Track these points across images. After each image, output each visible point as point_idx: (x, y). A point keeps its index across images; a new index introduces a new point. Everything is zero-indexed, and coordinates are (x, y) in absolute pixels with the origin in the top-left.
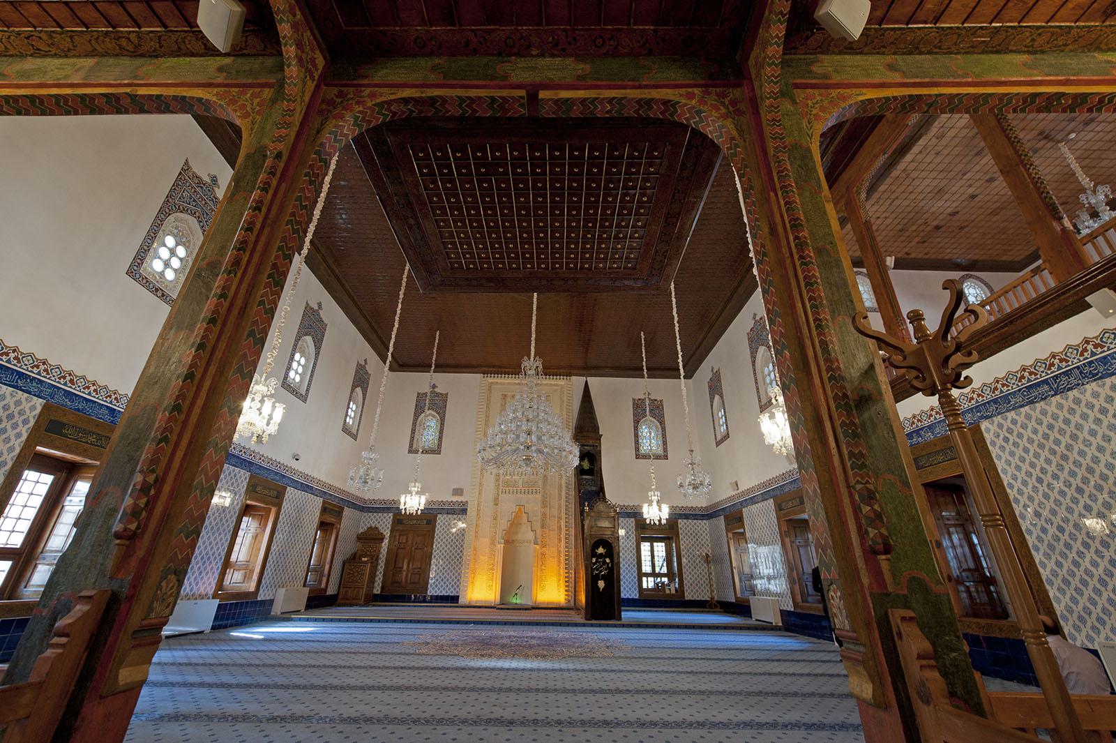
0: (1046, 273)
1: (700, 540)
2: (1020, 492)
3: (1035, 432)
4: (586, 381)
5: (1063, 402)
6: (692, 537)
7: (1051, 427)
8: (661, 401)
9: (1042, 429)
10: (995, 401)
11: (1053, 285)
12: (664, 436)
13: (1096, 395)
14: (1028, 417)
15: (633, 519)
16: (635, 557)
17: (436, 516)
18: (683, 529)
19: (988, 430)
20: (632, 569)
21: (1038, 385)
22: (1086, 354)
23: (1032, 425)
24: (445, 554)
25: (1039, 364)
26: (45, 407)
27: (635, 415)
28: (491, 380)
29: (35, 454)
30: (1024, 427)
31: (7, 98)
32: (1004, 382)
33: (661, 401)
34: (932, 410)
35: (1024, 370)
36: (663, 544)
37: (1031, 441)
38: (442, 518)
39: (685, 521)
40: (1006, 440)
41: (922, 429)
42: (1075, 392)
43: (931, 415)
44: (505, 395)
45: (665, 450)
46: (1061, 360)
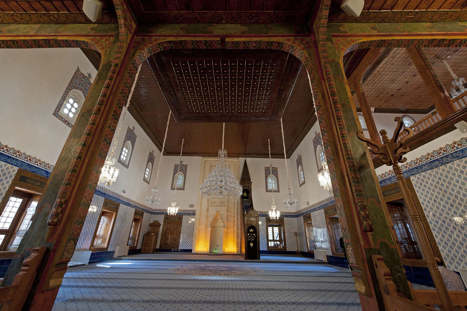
0: (438, 114)
1: (293, 226)
2: (427, 206)
3: (433, 181)
4: (245, 160)
5: (445, 168)
6: (289, 225)
7: (440, 179)
8: (277, 168)
9: (436, 180)
10: (416, 168)
11: (441, 119)
12: (278, 182)
13: (458, 165)
14: (430, 174)
15: (265, 217)
16: (266, 233)
17: (183, 216)
18: (286, 221)
19: (413, 180)
20: (264, 238)
21: (434, 161)
22: (454, 148)
23: (432, 178)
24: (186, 232)
25: (435, 152)
26: (19, 170)
27: (266, 174)
28: (205, 159)
29: (15, 190)
30: (429, 179)
31: (3, 41)
32: (420, 160)
33: (277, 168)
34: (390, 171)
35: (429, 155)
36: (278, 228)
37: (431, 185)
38: (185, 217)
39: (287, 218)
40: (421, 184)
41: (386, 180)
42: (450, 164)
43: (390, 174)
44: (212, 165)
45: (278, 188)
46: (444, 151)
